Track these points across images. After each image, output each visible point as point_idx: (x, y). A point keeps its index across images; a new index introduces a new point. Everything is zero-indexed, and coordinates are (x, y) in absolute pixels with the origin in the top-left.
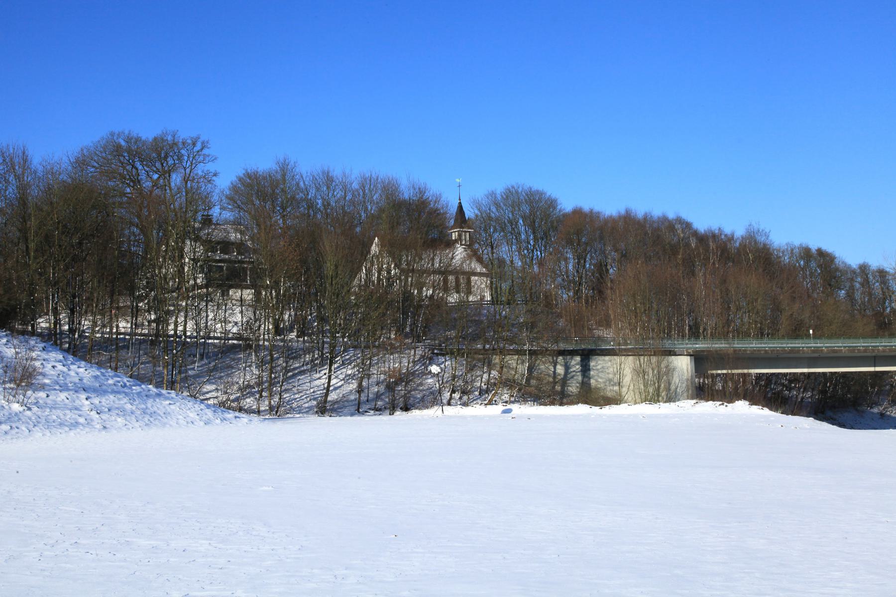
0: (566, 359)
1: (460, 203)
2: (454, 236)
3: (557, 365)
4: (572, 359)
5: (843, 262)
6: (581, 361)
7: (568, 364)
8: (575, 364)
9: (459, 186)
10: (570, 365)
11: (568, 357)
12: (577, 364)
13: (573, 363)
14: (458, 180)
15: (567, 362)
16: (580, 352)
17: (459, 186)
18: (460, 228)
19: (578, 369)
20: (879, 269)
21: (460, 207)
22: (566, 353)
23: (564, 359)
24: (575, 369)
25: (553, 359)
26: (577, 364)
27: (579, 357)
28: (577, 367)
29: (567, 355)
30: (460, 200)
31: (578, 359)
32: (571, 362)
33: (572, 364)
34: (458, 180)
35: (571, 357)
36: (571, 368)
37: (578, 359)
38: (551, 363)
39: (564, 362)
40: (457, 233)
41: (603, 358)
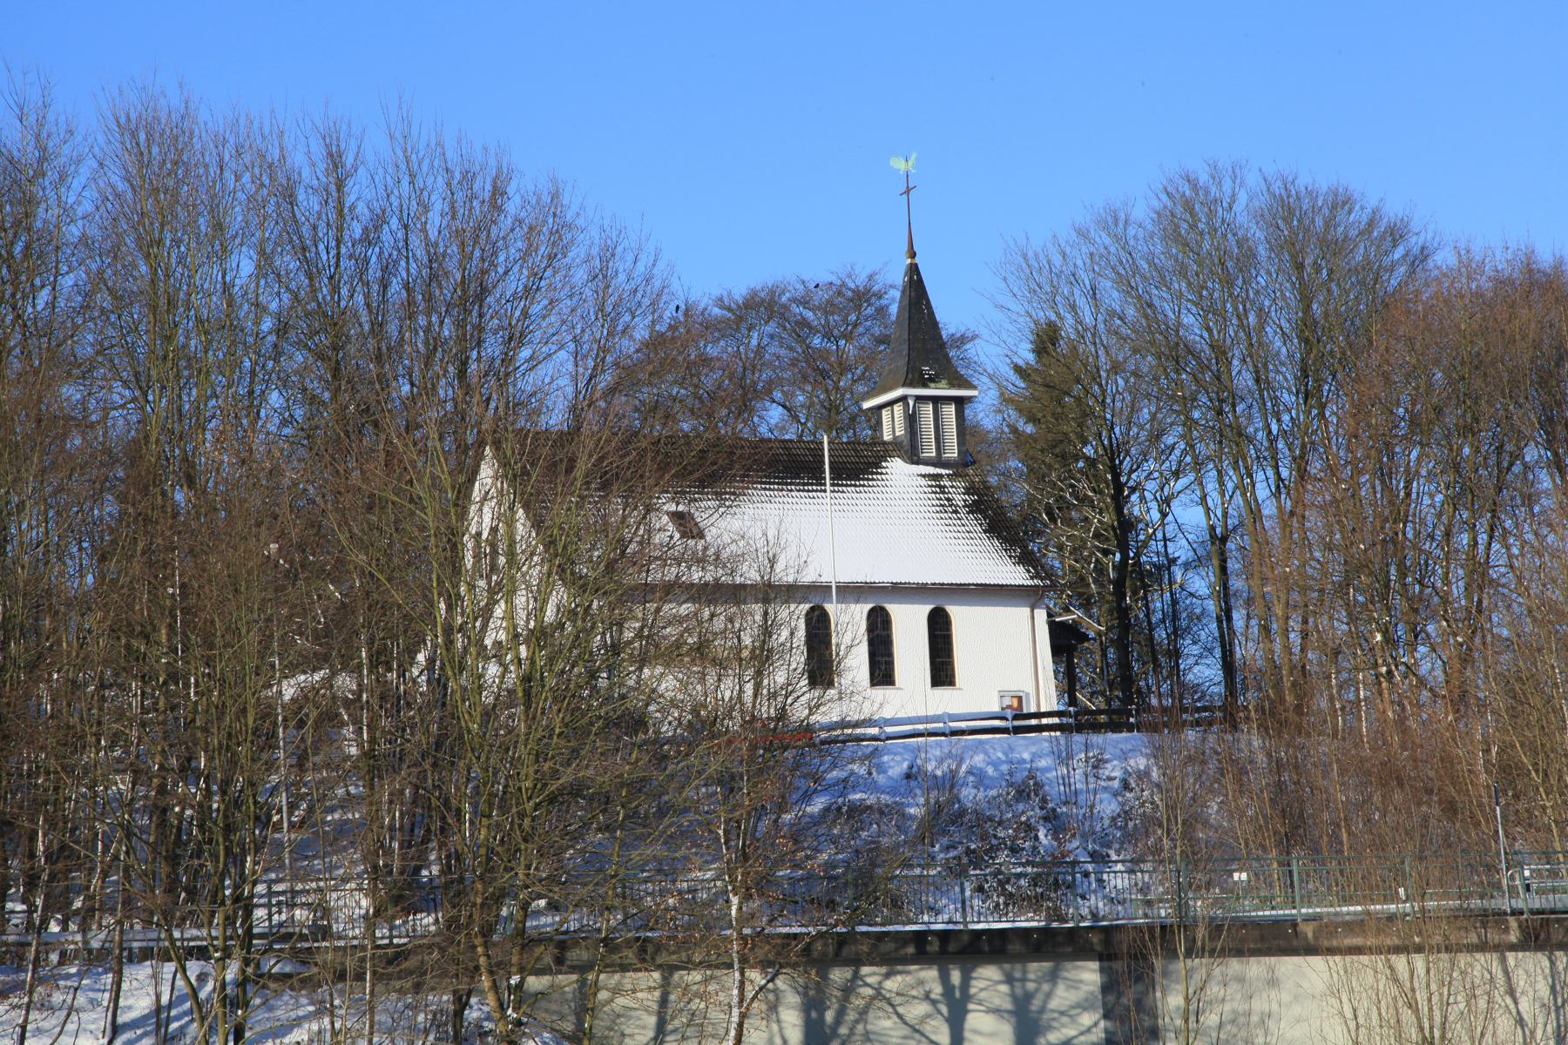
0: (1024, 980)
1: (914, 270)
2: (892, 426)
3: (966, 1012)
4: (1053, 977)
5: (720, 302)
6: (1106, 989)
7: (1036, 1004)
8: (1078, 1006)
9: (908, 191)
10: (1042, 1010)
11: (1036, 968)
12: (1084, 1006)
13: (1062, 997)
14: (899, 164)
15: (1029, 997)
16: (1095, 939)
17: (908, 191)
18: (911, 384)
19: (1089, 1030)
20: (1529, 269)
21: (915, 287)
22: (1015, 947)
23: (1009, 980)
24: (1073, 1033)
25: (945, 978)
26: (1084, 1006)
27: (1095, 965)
28: (1087, 1019)
29: (1023, 958)
30: (913, 255)
31: (1088, 975)
32: (1049, 995)
33: (1054, 1004)
34: (899, 164)
35: (1047, 965)
36: (1050, 1028)
37: (1088, 975)
38: (934, 1002)
39: (1013, 996)
40: (898, 408)
41: (1235, 965)
